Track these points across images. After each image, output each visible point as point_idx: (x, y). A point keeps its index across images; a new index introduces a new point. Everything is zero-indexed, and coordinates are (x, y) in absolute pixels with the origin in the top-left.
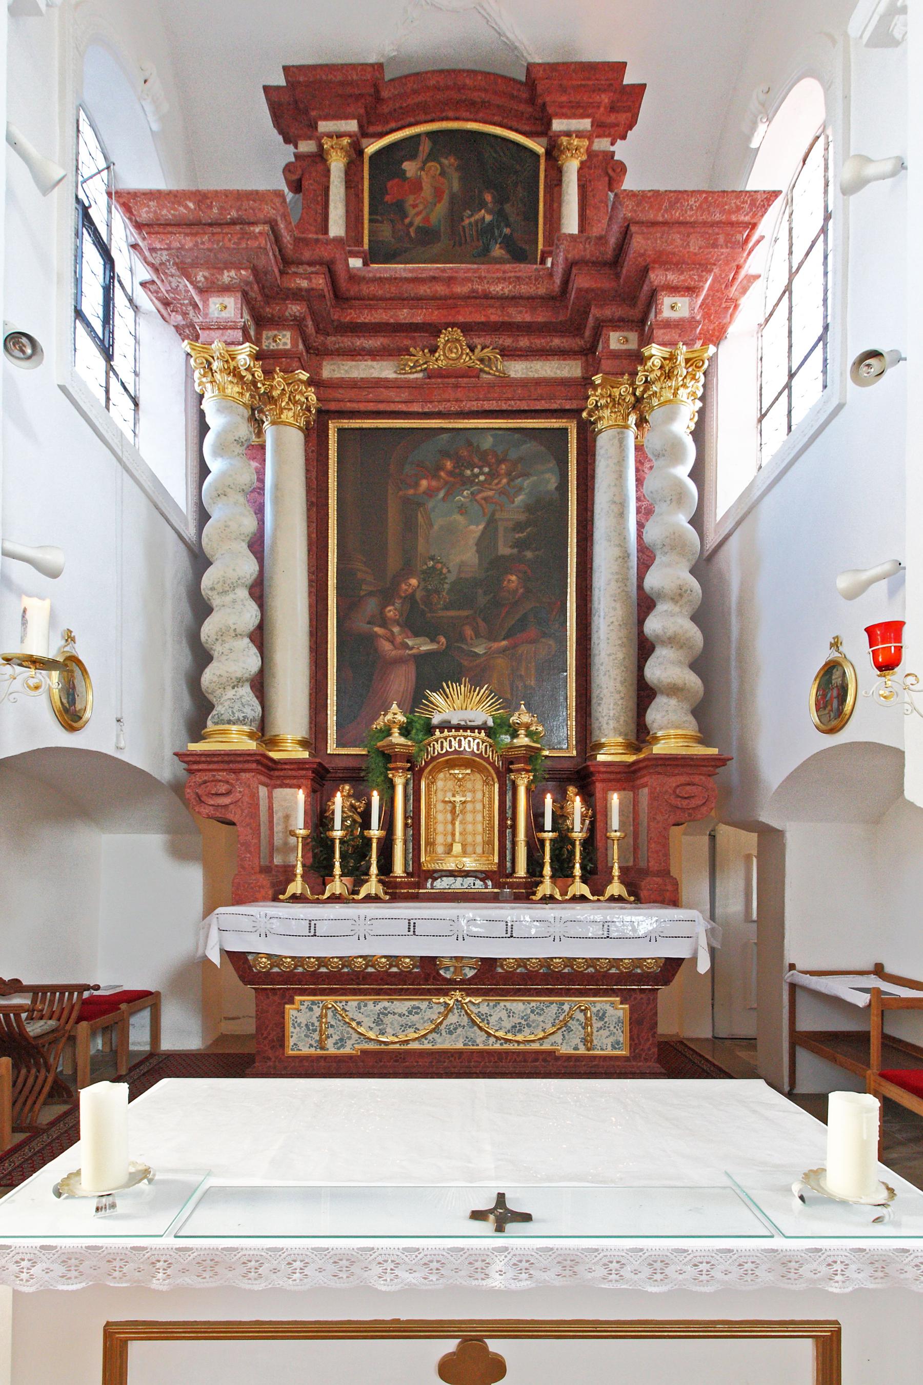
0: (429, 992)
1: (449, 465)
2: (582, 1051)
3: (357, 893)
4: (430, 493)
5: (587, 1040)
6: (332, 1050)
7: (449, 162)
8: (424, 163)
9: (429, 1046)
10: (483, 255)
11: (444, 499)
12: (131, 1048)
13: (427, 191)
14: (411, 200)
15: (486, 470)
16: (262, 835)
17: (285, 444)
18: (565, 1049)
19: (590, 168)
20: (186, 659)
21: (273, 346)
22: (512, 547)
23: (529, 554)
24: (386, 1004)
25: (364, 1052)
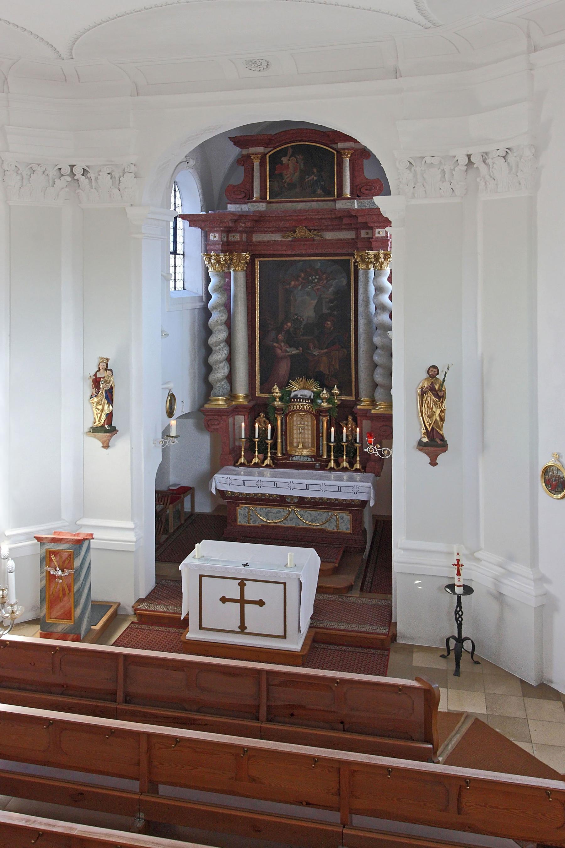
0: (284, 506)
1: (303, 275)
2: (335, 530)
3: (263, 463)
4: (296, 287)
5: (337, 526)
6: (252, 524)
7: (299, 157)
8: (290, 157)
9: (284, 525)
10: (314, 194)
11: (301, 290)
12: (185, 510)
13: (291, 169)
14: (285, 172)
15: (318, 277)
16: (230, 436)
17: (237, 278)
18: (330, 529)
19: (355, 155)
20: (203, 370)
21: (233, 239)
22: (328, 310)
23: (335, 313)
24: (269, 509)
25: (263, 526)
